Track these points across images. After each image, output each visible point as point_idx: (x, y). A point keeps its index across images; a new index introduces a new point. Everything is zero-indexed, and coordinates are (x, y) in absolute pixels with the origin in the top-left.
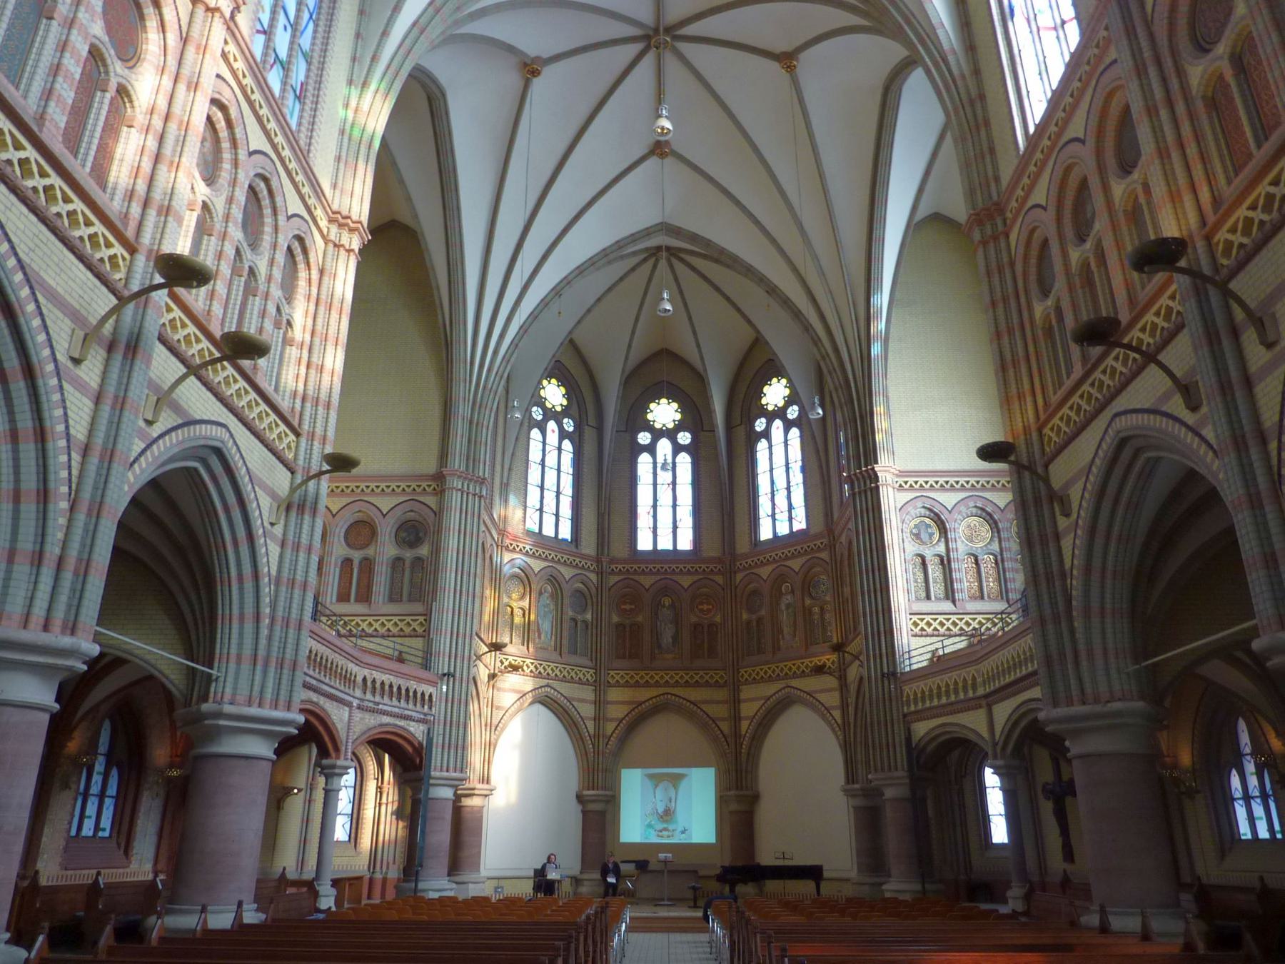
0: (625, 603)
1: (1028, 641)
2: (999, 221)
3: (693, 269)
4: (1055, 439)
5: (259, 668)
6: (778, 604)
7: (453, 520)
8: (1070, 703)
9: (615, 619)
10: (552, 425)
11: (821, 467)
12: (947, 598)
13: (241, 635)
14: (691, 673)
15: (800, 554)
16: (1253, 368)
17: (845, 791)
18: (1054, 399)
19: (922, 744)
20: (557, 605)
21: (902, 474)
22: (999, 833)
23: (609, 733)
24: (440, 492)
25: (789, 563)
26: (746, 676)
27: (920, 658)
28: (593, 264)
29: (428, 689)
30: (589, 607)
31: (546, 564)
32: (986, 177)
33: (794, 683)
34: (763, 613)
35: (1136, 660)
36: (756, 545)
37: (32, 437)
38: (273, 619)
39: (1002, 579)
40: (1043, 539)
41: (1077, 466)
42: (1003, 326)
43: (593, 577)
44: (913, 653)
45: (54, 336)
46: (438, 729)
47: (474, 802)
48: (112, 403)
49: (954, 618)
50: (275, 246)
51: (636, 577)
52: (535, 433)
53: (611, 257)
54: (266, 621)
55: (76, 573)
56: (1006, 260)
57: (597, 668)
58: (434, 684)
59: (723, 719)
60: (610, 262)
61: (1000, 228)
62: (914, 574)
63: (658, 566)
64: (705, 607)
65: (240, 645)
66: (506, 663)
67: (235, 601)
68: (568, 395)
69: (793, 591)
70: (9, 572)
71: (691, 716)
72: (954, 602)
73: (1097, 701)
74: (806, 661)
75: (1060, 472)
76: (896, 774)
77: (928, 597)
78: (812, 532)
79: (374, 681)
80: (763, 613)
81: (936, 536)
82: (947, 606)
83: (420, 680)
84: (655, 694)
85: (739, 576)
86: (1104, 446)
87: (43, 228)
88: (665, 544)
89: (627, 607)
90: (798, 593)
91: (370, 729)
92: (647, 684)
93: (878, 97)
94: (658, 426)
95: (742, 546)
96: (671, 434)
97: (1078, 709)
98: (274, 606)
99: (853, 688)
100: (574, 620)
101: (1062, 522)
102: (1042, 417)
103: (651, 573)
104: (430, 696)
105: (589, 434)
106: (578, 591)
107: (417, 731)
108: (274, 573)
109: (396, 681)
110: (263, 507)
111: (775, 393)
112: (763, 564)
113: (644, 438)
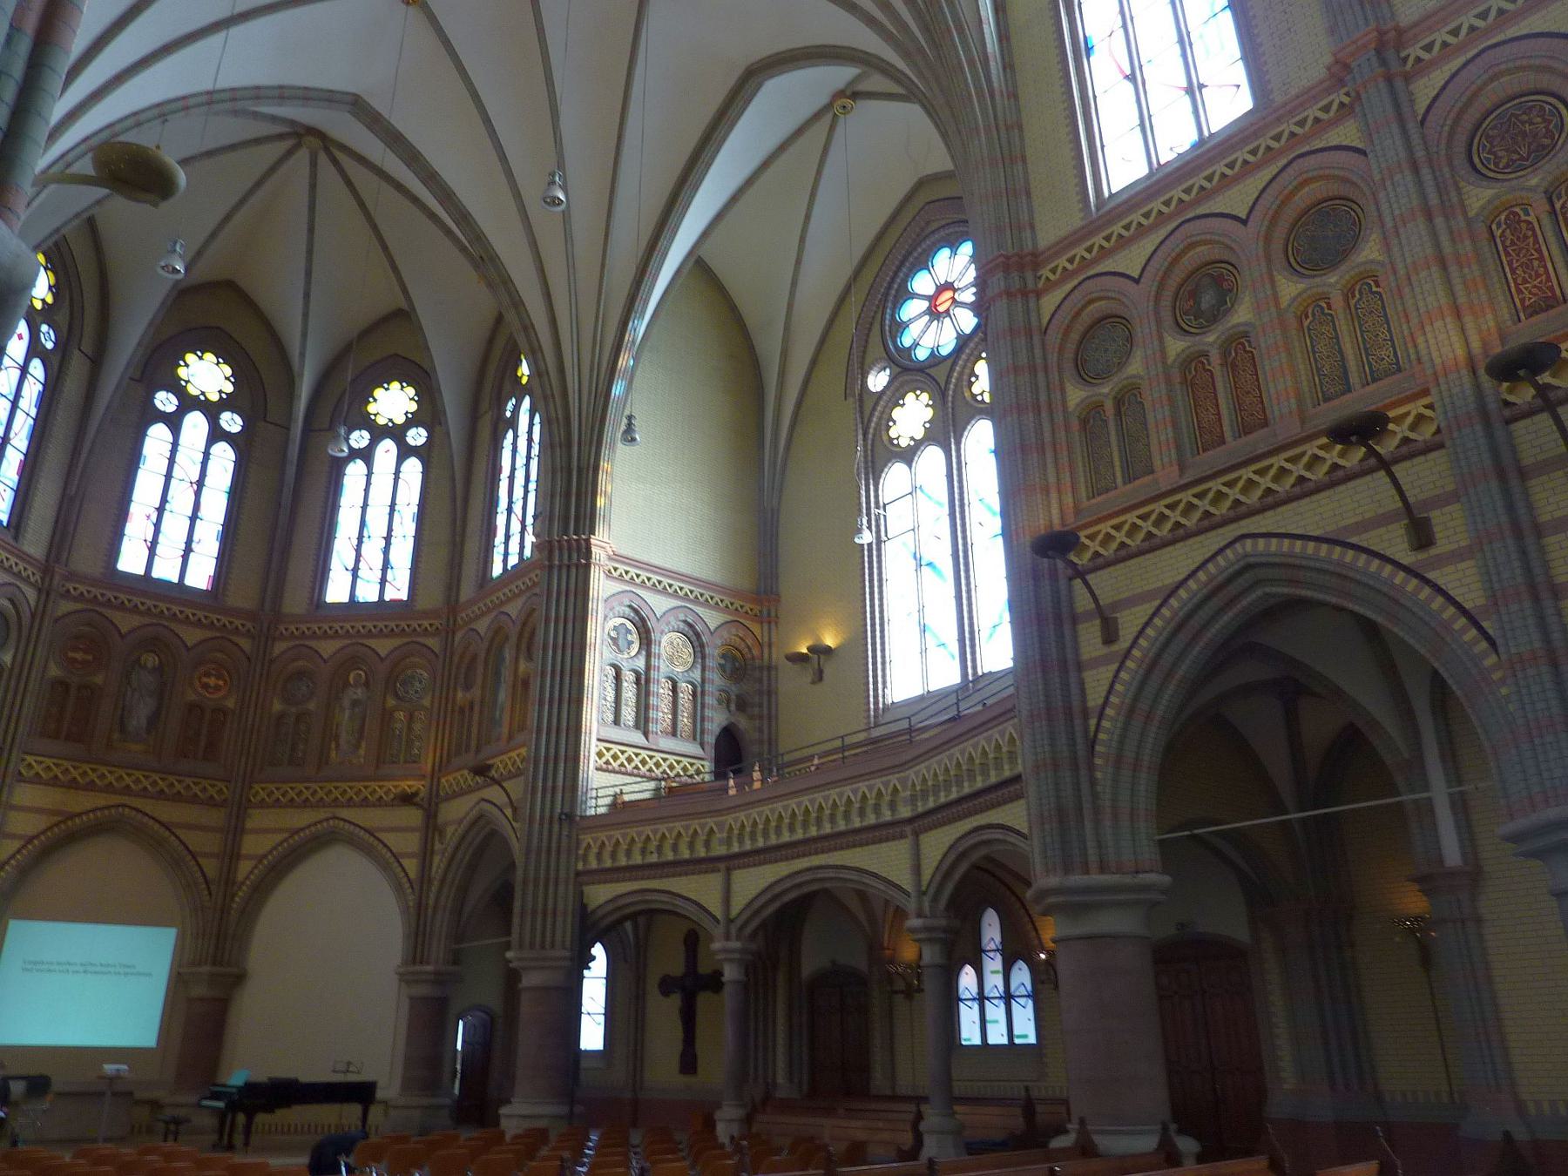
0: (75, 649)
9: (54, 671)
12: (637, 726)
14: (171, 779)
19: (600, 913)
21: (616, 557)
22: (592, 1036)
25: (372, 643)
26: (263, 794)
28: (210, 103)
30: (12, 642)
33: (345, 813)
34: (312, 706)
36: (318, 606)
39: (698, 717)
43: (31, 594)
49: (644, 754)
51: (108, 612)
53: (240, 105)
60: (235, 113)
64: (212, 681)
69: (367, 684)
72: (646, 734)
73: (1119, 870)
80: (312, 706)
81: (636, 647)
82: (637, 738)
84: (88, 805)
85: (280, 647)
88: (166, 570)
89: (79, 656)
92: (91, 787)
93: (732, 81)
94: (192, 390)
95: (295, 603)
96: (212, 411)
97: (1097, 878)
103: (135, 610)
105: (78, 366)
111: (393, 402)
112: (325, 636)
113: (165, 401)
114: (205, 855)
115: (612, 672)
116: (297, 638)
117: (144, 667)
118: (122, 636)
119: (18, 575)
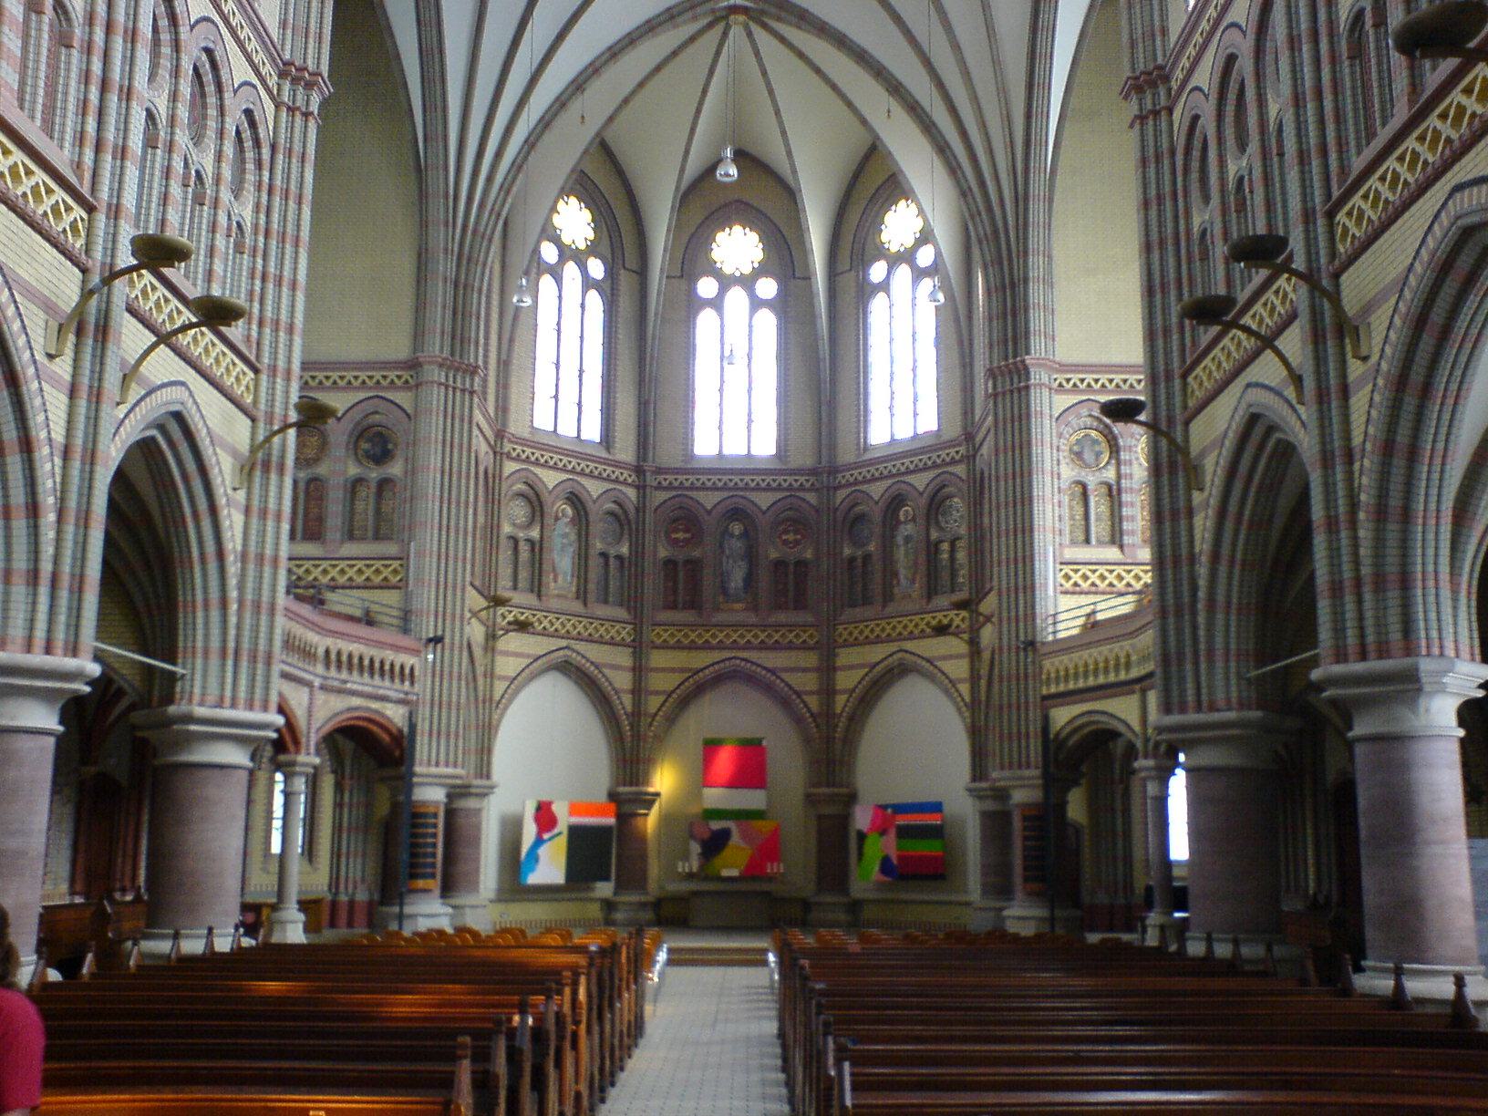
0: (677, 531)
1: (1148, 639)
2: (1162, 91)
3: (783, 40)
4: (1353, 230)
5: (230, 662)
6: (893, 537)
7: (433, 427)
8: (1183, 710)
9: (663, 553)
10: (571, 270)
11: (961, 343)
12: (1113, 542)
13: (206, 623)
15: (926, 468)
16: (1351, 378)
17: (970, 790)
18: (1358, 164)
19: (1064, 734)
20: (579, 535)
23: (653, 711)
24: (415, 386)
25: (909, 479)
27: (1071, 624)
29: (409, 660)
31: (565, 476)
32: (1152, 25)
33: (909, 645)
34: (872, 548)
35: (1261, 659)
37: (17, 449)
38: (241, 602)
40: (1175, 515)
41: (1214, 430)
42: (1155, 237)
43: (631, 493)
44: (1061, 617)
45: (32, 340)
46: (423, 713)
47: (471, 803)
48: (87, 394)
49: (1119, 569)
50: (221, 134)
52: (546, 282)
54: (234, 607)
55: (71, 591)
56: (1165, 145)
57: (637, 623)
58: (416, 652)
59: (811, 693)
61: (1163, 101)
62: (1071, 508)
63: (725, 478)
64: (791, 537)
65: (207, 636)
66: (510, 618)
67: (199, 583)
68: (597, 223)
70: (7, 593)
71: (768, 689)
74: (928, 617)
75: (1357, 286)
76: (1027, 773)
77: (1087, 541)
78: (946, 437)
79: (339, 654)
80: (872, 548)
81: (1106, 457)
82: (1112, 553)
83: (397, 648)
84: (708, 661)
86: (1431, 243)
87: (13, 216)
89: (680, 535)
90: (921, 521)
91: (336, 715)
92: (707, 646)
96: (747, 282)
97: (1192, 717)
98: (241, 587)
99: (986, 655)
100: (604, 555)
101: (1355, 369)
102: (1336, 194)
103: (715, 488)
104: (412, 669)
105: (626, 281)
106: (611, 513)
107: (396, 715)
108: (239, 548)
109: (368, 652)
110: (224, 469)
111: (899, 225)
112: (874, 479)
114: (807, 693)
115: (1078, 489)
116: (1082, 392)
117: (732, 535)
118: (709, 512)
119: (616, 481)
